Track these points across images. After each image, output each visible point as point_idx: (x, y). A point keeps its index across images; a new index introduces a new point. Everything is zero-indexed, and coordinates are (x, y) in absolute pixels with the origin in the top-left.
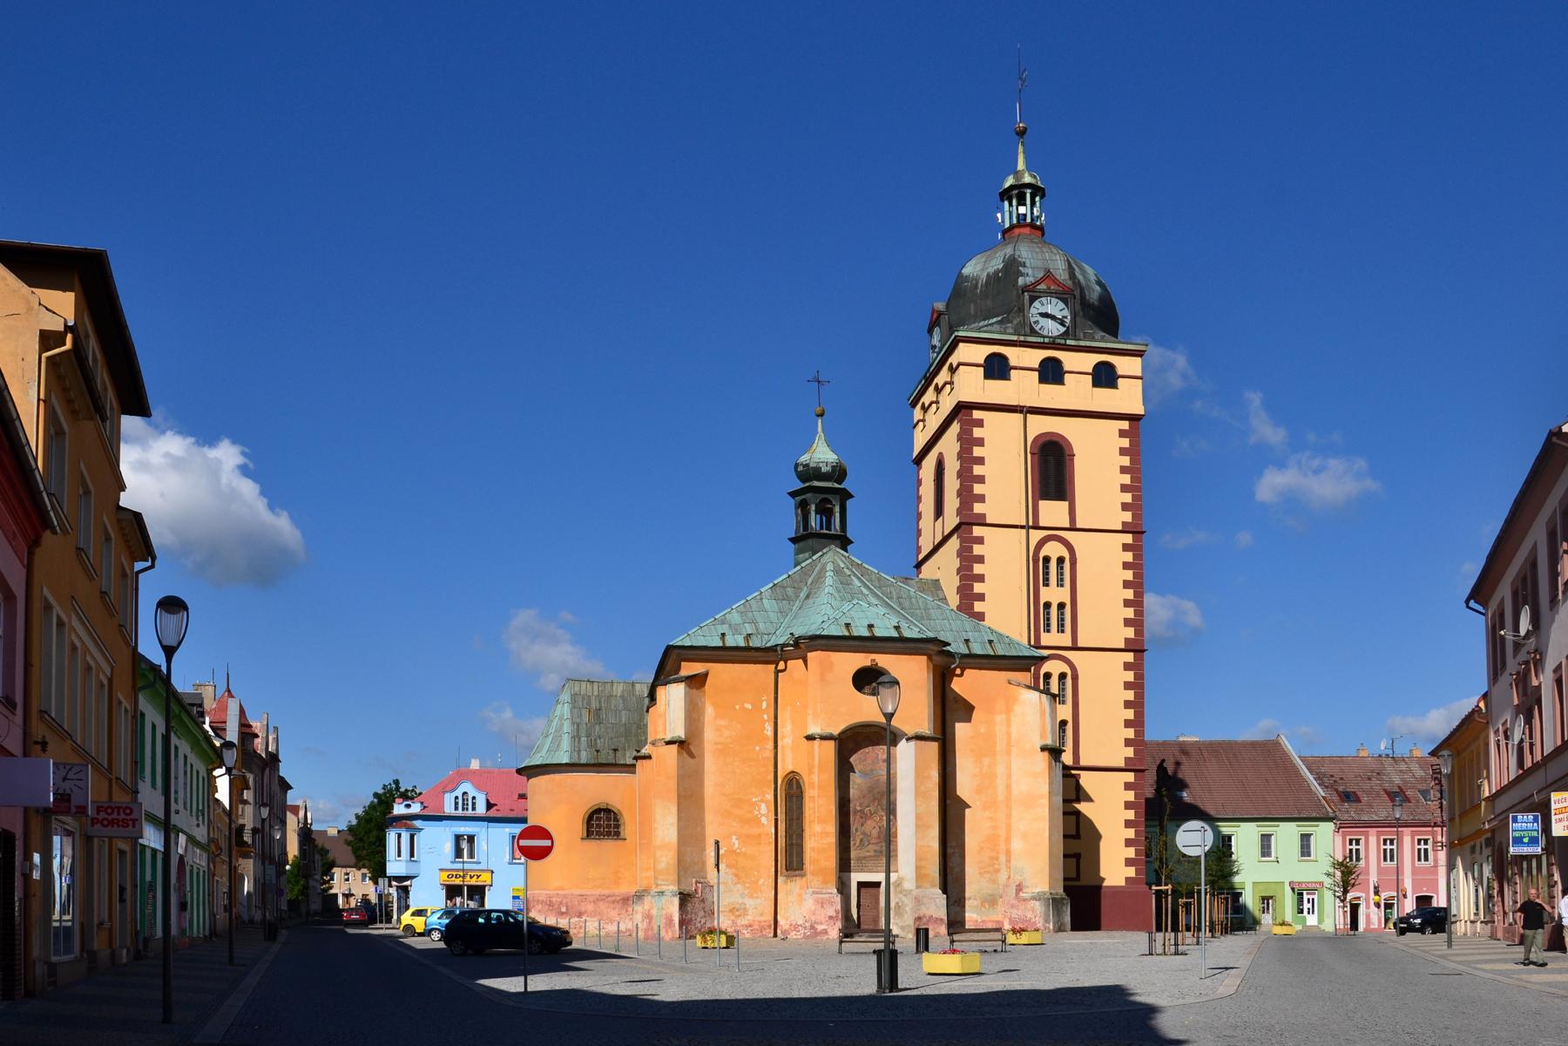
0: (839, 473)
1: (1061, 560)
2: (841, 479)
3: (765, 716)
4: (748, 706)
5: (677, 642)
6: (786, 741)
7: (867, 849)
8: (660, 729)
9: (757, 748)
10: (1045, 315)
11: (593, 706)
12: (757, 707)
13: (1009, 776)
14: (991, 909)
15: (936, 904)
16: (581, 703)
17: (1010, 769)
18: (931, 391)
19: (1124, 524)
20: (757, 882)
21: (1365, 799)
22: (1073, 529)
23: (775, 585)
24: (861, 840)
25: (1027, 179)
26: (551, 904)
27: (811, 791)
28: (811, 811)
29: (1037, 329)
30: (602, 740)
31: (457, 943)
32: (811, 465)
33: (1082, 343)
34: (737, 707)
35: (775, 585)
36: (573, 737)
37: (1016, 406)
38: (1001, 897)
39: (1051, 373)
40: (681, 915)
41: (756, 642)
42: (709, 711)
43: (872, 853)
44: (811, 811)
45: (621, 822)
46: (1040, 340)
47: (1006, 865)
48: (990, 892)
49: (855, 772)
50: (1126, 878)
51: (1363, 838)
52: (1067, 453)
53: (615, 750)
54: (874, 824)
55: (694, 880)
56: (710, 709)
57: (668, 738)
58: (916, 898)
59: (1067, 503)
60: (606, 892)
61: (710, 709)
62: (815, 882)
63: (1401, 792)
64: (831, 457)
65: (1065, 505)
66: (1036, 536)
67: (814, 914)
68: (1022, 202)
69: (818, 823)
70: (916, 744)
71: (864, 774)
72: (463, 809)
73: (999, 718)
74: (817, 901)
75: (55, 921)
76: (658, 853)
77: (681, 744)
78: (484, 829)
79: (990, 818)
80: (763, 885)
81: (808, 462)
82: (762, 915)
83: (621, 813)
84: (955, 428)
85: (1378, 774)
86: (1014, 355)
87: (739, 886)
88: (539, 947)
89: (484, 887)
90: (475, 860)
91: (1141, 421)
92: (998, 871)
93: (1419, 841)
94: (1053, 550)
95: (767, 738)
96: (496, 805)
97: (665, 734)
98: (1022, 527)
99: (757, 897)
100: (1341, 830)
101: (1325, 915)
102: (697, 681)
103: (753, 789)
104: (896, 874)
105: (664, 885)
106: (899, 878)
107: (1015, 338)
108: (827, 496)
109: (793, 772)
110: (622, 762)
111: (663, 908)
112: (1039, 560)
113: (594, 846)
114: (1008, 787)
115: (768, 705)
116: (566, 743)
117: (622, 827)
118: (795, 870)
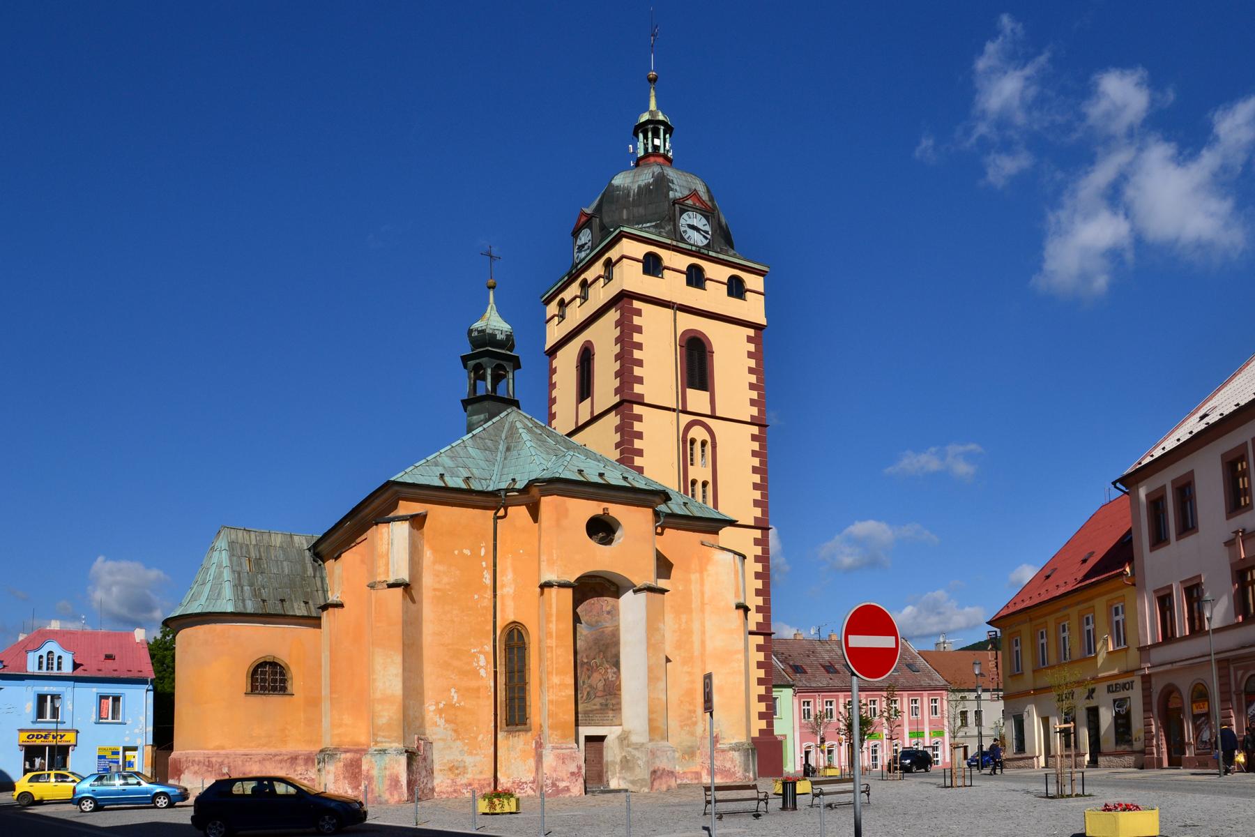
0: (508, 342)
1: (704, 444)
2: (511, 348)
3: (484, 564)
4: (467, 552)
5: (398, 477)
6: (507, 588)
7: (593, 702)
8: (381, 570)
9: (476, 597)
10: (692, 227)
11: (253, 555)
12: (475, 553)
13: (703, 633)
14: (691, 760)
15: (668, 757)
16: (239, 551)
17: (704, 627)
18: (574, 289)
19: (752, 417)
20: (476, 738)
21: (809, 671)
22: (713, 416)
23: (474, 435)
24: (588, 693)
25: (661, 117)
26: (210, 765)
27: (548, 641)
28: (549, 662)
29: (686, 237)
30: (266, 590)
31: (215, 824)
32: (487, 331)
33: (721, 256)
34: (456, 552)
35: (474, 435)
36: (235, 586)
37: (670, 302)
38: (699, 749)
39: (695, 278)
40: (408, 775)
41: (475, 486)
42: (428, 555)
43: (598, 707)
44: (549, 662)
45: (289, 676)
47: (702, 718)
48: (689, 744)
49: (581, 623)
50: (760, 730)
51: (812, 700)
52: (708, 349)
53: (282, 601)
54: (599, 677)
55: (416, 736)
56: (428, 553)
57: (391, 580)
58: (651, 752)
59: (708, 393)
60: (273, 751)
61: (428, 553)
63: (832, 666)
64: (506, 327)
65: (706, 395)
67: (555, 771)
68: (656, 134)
69: (556, 675)
71: (590, 625)
72: (48, 669)
73: (694, 577)
74: (558, 756)
76: (378, 707)
77: (406, 586)
78: (69, 689)
79: (688, 673)
81: (484, 328)
82: (481, 772)
83: (288, 667)
84: (613, 315)
85: (813, 652)
86: (668, 257)
87: (459, 743)
88: (333, 825)
89: (68, 747)
90: (120, 721)
91: (764, 331)
93: (932, 700)
94: (698, 433)
95: (486, 586)
96: (82, 665)
97: (388, 576)
98: (674, 410)
99: (477, 754)
100: (798, 694)
101: (788, 761)
102: (417, 521)
104: (621, 727)
105: (385, 742)
106: (623, 731)
107: (669, 241)
108: (501, 362)
109: (514, 622)
110: (291, 613)
111: (385, 768)
112: (687, 441)
113: (257, 701)
114: (703, 643)
115: (486, 553)
116: (228, 591)
118: (517, 725)
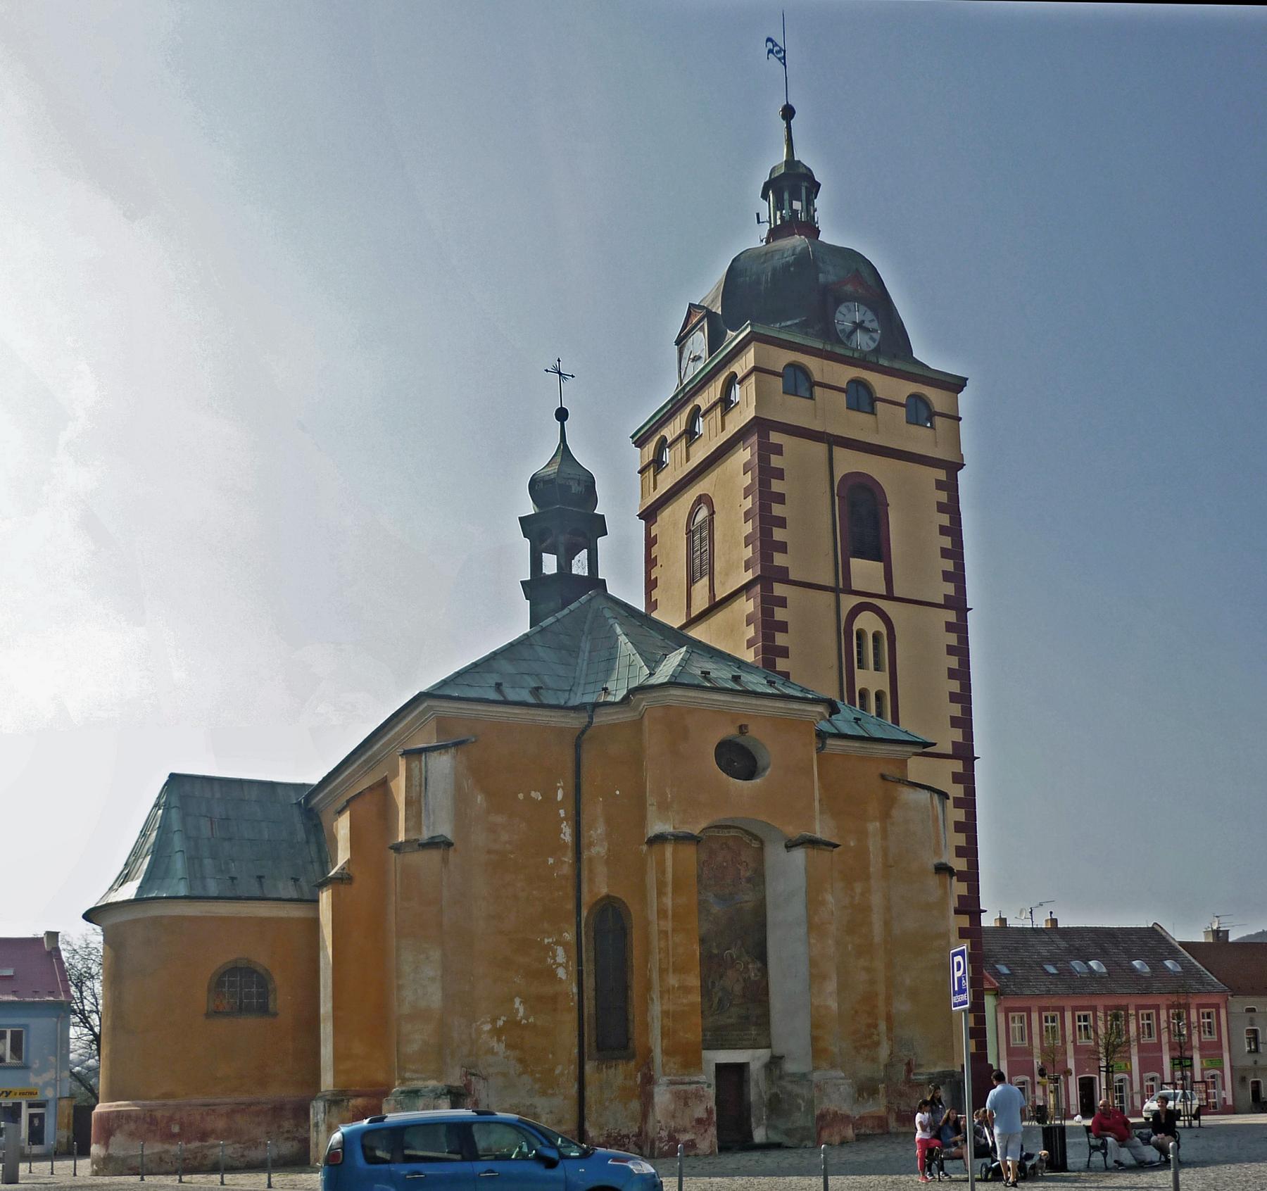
3: (562, 812)
4: (536, 795)
22: (890, 597)
34: (521, 796)
39: (861, 398)
46: (849, 353)
60: (245, 1098)
62: (672, 1065)
66: (849, 602)
69: (674, 971)
70: (807, 853)
75: (853, 354)
80: (562, 1074)
92: (877, 1044)
95: (565, 845)
103: (546, 925)
105: (417, 1079)
117: (271, 997)
